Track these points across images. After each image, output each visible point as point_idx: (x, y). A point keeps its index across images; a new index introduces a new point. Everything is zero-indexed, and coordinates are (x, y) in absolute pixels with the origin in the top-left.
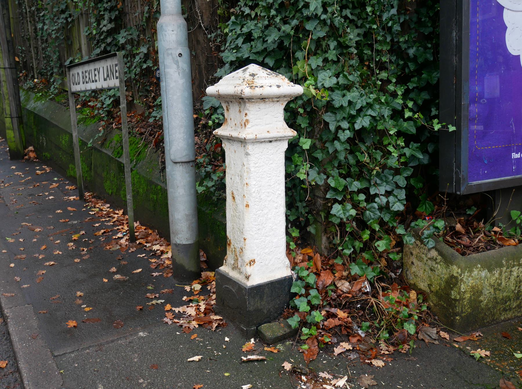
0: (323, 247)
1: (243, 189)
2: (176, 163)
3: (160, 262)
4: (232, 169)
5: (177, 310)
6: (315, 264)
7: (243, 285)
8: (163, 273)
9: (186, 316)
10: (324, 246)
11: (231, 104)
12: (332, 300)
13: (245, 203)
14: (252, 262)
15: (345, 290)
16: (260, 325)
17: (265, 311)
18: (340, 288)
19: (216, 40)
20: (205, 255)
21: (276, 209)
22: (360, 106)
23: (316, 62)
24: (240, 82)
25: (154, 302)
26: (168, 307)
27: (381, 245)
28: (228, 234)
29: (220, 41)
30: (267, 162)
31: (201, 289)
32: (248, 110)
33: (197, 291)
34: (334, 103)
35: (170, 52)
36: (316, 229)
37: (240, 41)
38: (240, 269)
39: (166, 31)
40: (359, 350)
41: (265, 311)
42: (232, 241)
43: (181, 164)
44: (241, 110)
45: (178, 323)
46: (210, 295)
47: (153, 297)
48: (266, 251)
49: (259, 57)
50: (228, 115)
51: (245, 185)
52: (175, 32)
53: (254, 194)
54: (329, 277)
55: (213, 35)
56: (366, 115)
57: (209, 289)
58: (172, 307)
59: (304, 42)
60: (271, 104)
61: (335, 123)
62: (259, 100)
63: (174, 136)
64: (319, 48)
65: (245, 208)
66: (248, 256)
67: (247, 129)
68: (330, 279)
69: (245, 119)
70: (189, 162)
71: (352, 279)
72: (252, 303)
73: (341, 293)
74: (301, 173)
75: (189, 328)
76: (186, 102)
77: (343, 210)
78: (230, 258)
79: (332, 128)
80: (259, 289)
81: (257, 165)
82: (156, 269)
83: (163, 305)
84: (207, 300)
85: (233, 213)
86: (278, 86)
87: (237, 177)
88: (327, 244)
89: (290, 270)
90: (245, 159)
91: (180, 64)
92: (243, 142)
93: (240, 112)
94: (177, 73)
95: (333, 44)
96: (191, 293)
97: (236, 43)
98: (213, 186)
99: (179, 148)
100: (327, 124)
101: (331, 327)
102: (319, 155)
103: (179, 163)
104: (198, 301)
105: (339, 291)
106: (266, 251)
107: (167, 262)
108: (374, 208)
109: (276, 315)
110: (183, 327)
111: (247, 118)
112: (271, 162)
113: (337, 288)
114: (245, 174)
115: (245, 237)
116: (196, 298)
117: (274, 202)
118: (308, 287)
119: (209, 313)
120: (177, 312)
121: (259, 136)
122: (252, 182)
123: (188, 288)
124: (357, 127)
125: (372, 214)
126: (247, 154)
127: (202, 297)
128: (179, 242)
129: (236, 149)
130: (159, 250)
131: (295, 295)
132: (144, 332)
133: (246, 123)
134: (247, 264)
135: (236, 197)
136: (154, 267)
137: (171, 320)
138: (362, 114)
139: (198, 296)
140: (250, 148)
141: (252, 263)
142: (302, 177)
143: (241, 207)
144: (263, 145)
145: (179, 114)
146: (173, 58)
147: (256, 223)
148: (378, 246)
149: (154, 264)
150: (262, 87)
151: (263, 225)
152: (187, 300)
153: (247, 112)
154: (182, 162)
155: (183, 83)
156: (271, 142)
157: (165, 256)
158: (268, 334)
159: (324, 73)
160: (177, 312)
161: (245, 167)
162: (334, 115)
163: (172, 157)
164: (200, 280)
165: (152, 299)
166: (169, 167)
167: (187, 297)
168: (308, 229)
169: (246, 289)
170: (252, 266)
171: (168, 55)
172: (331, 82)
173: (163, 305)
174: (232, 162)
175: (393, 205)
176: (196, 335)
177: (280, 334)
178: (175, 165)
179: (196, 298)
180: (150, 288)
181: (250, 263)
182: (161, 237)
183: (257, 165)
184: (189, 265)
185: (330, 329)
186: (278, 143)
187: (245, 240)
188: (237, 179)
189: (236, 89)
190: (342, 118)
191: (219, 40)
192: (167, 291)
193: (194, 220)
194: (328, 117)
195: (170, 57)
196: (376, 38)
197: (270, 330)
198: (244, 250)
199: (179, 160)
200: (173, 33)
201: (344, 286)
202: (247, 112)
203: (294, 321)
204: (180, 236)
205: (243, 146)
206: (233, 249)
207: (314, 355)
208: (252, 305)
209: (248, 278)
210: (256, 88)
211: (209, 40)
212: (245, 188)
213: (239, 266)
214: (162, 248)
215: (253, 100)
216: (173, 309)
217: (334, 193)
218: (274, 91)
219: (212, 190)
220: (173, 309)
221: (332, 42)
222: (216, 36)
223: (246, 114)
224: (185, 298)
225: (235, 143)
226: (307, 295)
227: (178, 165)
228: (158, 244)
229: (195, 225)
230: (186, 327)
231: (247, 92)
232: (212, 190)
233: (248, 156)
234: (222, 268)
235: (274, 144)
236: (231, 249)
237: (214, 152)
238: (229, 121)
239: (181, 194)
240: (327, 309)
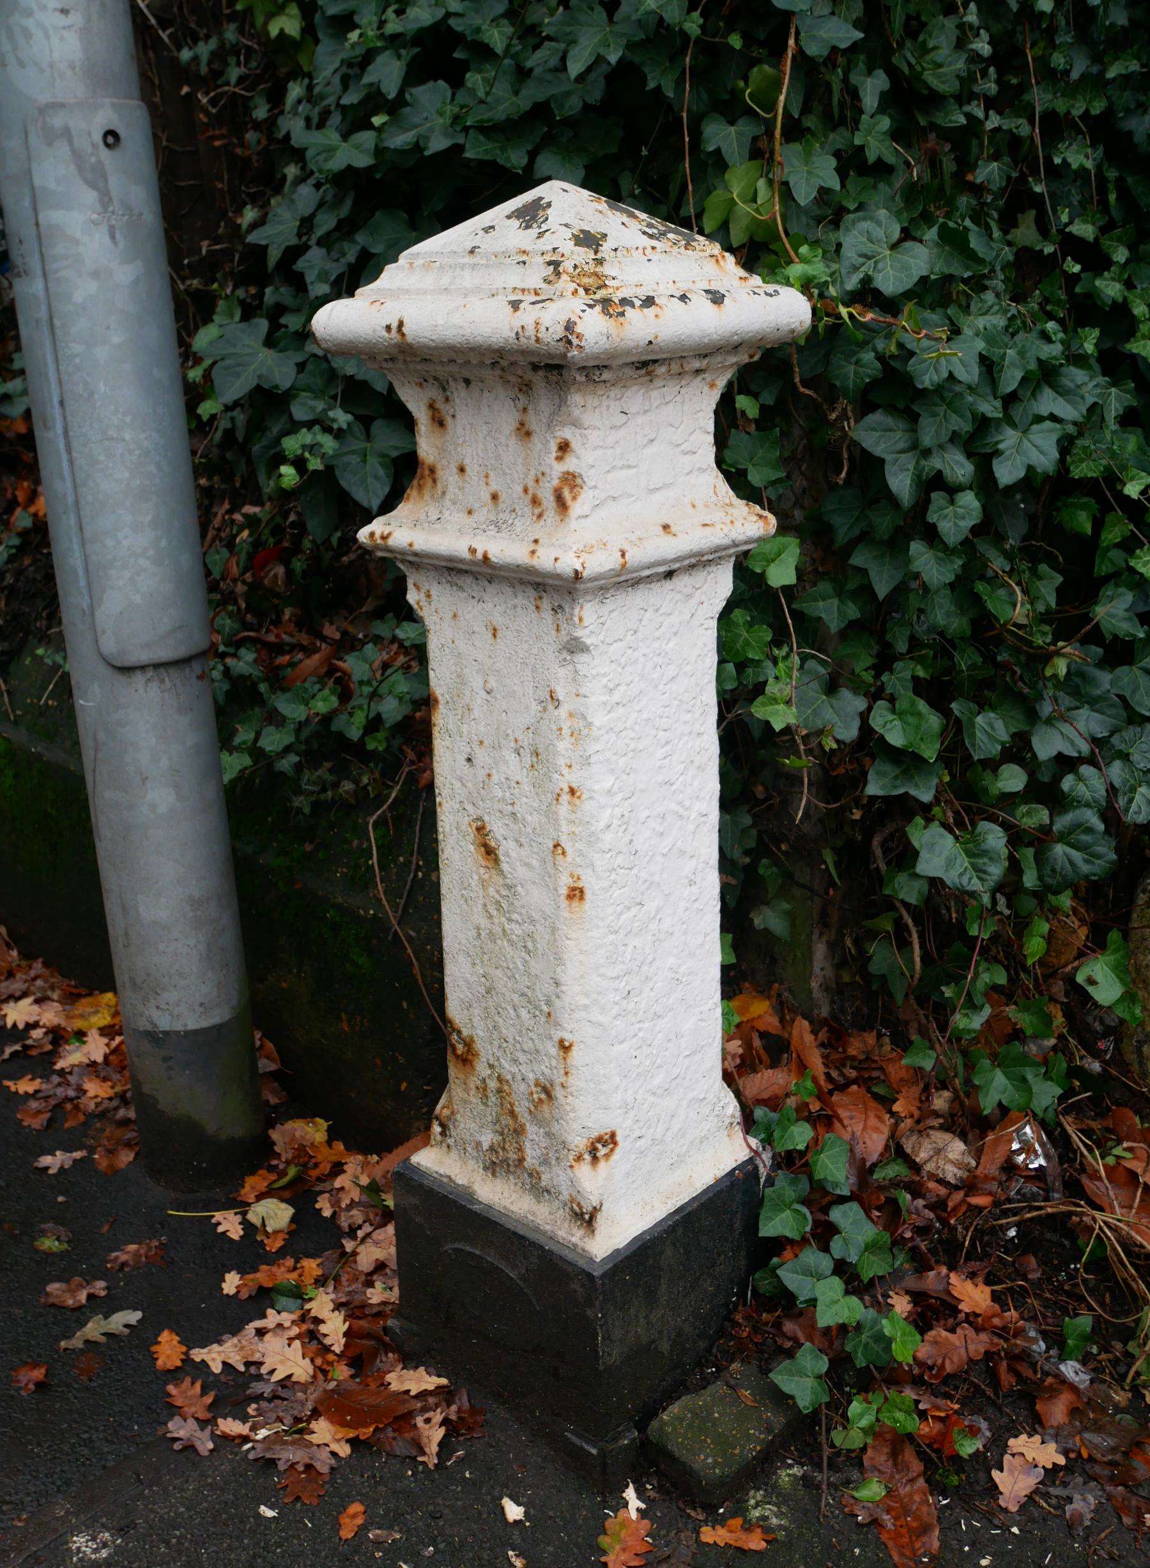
0: (814, 984)
1: (550, 815)
2: (127, 670)
3: (60, 1091)
4: (476, 713)
5: (215, 1356)
6: (815, 1080)
7: (570, 1256)
8: (92, 1150)
9: (267, 1390)
10: (820, 980)
11: (459, 394)
12: (935, 1235)
13: (565, 882)
14: (602, 1145)
15: (951, 1173)
16: (651, 1411)
17: (665, 1346)
18: (929, 1167)
19: (221, 73)
20: (270, 1045)
21: (692, 883)
22: (1019, 375)
23: (812, 172)
24: (535, 276)
25: (94, 1329)
26: (168, 1349)
27: (1099, 978)
28: (453, 1009)
29: (241, 80)
30: (656, 675)
31: (293, 1220)
32: (576, 424)
33: (276, 1232)
34: (912, 365)
35: (58, 121)
36: (791, 916)
37: (388, 73)
38: (534, 1175)
39: (29, 13)
40: (1091, 1459)
41: (665, 1346)
42: (479, 1045)
43: (150, 673)
44: (533, 423)
45: (246, 1439)
46: (344, 1253)
47: (82, 1297)
48: (656, 1082)
49: (503, 149)
50: (442, 450)
51: (565, 797)
52: (76, 19)
53: (608, 837)
54: (873, 1121)
55: (204, 50)
56: (1039, 419)
57: (327, 1213)
58: (190, 1341)
59: (761, 72)
60: (671, 390)
61: (909, 461)
62: (629, 372)
63: (109, 543)
64: (825, 102)
65: (563, 902)
66: (582, 1117)
67: (573, 523)
68: (877, 1130)
69: (558, 469)
70: (186, 661)
71: (973, 1124)
72: (617, 1334)
73: (943, 1191)
74: (774, 700)
75: (309, 1467)
76: (156, 373)
77: (970, 854)
78: (464, 1105)
79: (901, 482)
80: (643, 1254)
81: (616, 696)
82: (54, 1134)
83: (141, 1338)
84: (337, 1279)
85: (484, 923)
86: (717, 298)
87: (512, 758)
88: (830, 973)
89: (741, 1135)
90: (562, 672)
91: (115, 182)
92: (553, 591)
93: (524, 432)
94: (104, 229)
95: (872, 87)
96: (250, 1251)
97: (367, 79)
98: (288, 749)
99: (138, 599)
100: (870, 467)
101: (949, 1368)
102: (831, 611)
103: (143, 668)
104: (298, 1294)
105: (932, 1185)
106: (656, 1082)
107: (95, 1089)
108: (1089, 830)
109: (702, 1344)
110: (282, 1466)
111: (571, 464)
112: (671, 671)
113: (916, 1167)
114: (563, 745)
115: (568, 1037)
116: (282, 1273)
117: (682, 853)
118: (820, 1199)
119: (374, 1356)
120: (217, 1368)
121: (636, 556)
122: (598, 781)
123: (229, 1224)
124: (1007, 473)
125: (1076, 855)
126: (575, 647)
127: (311, 1266)
128: (164, 1023)
129: (499, 621)
130: (36, 1025)
131: (778, 1245)
132: (91, 1526)
133: (567, 494)
134: (579, 1158)
135: (507, 849)
136: (37, 1123)
137: (203, 1424)
138: (1017, 412)
139: (290, 1262)
140: (593, 619)
141: (602, 1151)
142: (780, 717)
143: (535, 897)
144: (639, 598)
145: (128, 436)
146: (78, 157)
147: (618, 970)
148: (1092, 982)
149: (34, 1105)
150: (649, 302)
151: (645, 968)
152: (244, 1295)
153: (567, 433)
154: (157, 666)
155: (136, 282)
156: (669, 575)
157: (72, 1057)
158: (706, 1461)
159: (866, 225)
160: (217, 1368)
161: (563, 712)
162: (901, 425)
163: (109, 645)
164: (272, 1169)
165: (80, 1315)
166: (96, 689)
167: (242, 1272)
168: (758, 922)
169: (590, 1276)
170: (602, 1164)
171: (50, 136)
172: (905, 268)
173: (141, 1338)
174: (476, 683)
175: (1131, 800)
176: (356, 1508)
177: (753, 1449)
178: (122, 679)
179: (282, 1273)
180: (49, 1244)
181: (593, 1151)
182: (28, 955)
183: (616, 696)
184: (205, 1104)
185: (948, 1379)
186: (699, 576)
187: (565, 1048)
188: (513, 766)
189: (528, 316)
190: (945, 437)
191: (234, 73)
192: (136, 1255)
193: (226, 918)
194: (877, 435)
195: (62, 149)
196: (1043, 62)
197: (707, 1425)
198: (558, 1092)
199: (145, 657)
200: (62, 20)
201: (947, 1156)
202: (567, 433)
203: (802, 1380)
204: (170, 996)
205: (546, 604)
206: (493, 1084)
207: (925, 1529)
208: (618, 1337)
209: (587, 1219)
210: (629, 311)
211: (185, 73)
212: (563, 810)
213: (530, 1161)
214: (51, 1015)
215: (606, 375)
216: (198, 1354)
217: (891, 770)
218: (698, 322)
219: (286, 764)
220: (198, 1354)
221: (870, 73)
222: (220, 56)
223: (564, 447)
224: (231, 1283)
225: (492, 589)
226: (824, 1233)
227: (139, 678)
228: (25, 994)
229: (230, 939)
230: (292, 1466)
231: (595, 330)
232: (286, 764)
233: (581, 658)
234: (429, 1159)
235: (682, 582)
236: (474, 1081)
237: (254, 587)
238: (448, 476)
239: (162, 809)
240: (911, 1282)
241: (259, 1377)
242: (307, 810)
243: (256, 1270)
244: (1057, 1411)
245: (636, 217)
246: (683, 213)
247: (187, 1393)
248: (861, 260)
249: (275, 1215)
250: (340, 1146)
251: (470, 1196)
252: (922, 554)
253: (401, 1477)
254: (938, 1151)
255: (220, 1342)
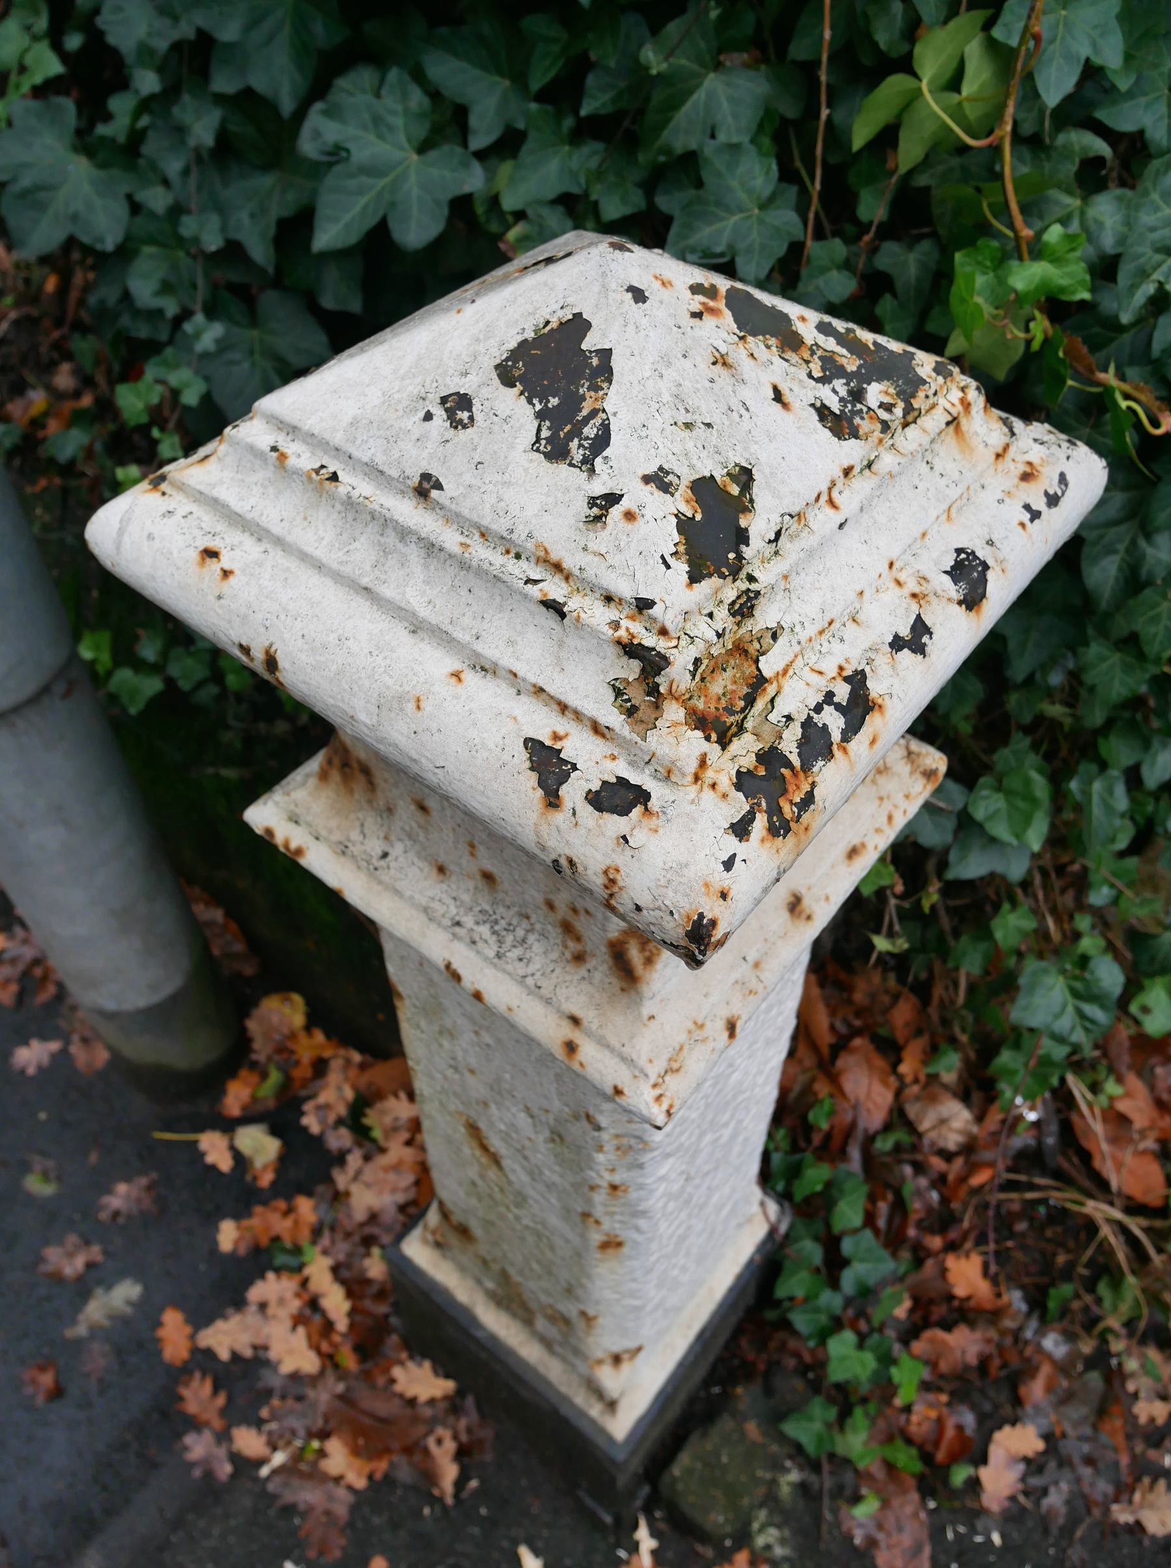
18: (933, 1135)
133: (635, 955)
224: (228, 1235)
241: (267, 1363)
242: (238, 745)
243: (249, 1214)
244: (1036, 1390)
245: (791, 341)
246: (798, 50)
247: (198, 1396)
248: (1158, 257)
249: (260, 1146)
250: (319, 1037)
251: (474, 1320)
252: (1103, 659)
253: (418, 1514)
254: (943, 1122)
255: (225, 1317)
